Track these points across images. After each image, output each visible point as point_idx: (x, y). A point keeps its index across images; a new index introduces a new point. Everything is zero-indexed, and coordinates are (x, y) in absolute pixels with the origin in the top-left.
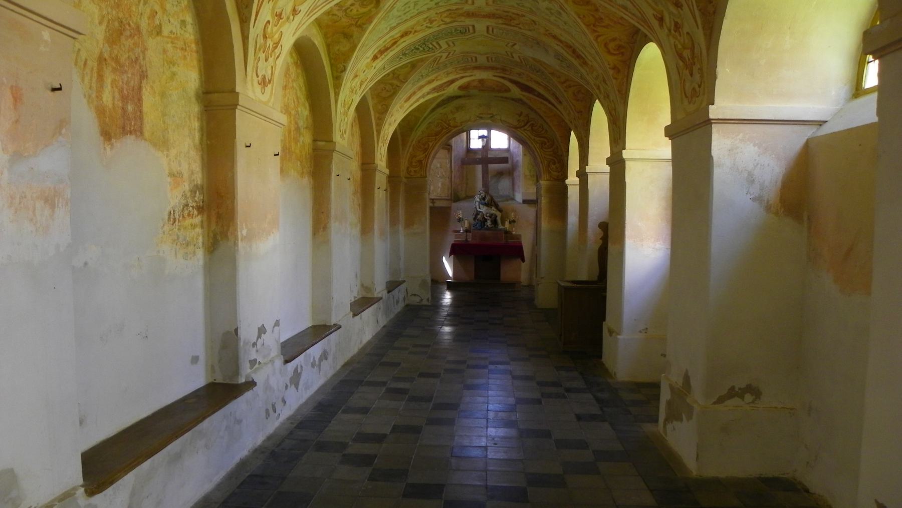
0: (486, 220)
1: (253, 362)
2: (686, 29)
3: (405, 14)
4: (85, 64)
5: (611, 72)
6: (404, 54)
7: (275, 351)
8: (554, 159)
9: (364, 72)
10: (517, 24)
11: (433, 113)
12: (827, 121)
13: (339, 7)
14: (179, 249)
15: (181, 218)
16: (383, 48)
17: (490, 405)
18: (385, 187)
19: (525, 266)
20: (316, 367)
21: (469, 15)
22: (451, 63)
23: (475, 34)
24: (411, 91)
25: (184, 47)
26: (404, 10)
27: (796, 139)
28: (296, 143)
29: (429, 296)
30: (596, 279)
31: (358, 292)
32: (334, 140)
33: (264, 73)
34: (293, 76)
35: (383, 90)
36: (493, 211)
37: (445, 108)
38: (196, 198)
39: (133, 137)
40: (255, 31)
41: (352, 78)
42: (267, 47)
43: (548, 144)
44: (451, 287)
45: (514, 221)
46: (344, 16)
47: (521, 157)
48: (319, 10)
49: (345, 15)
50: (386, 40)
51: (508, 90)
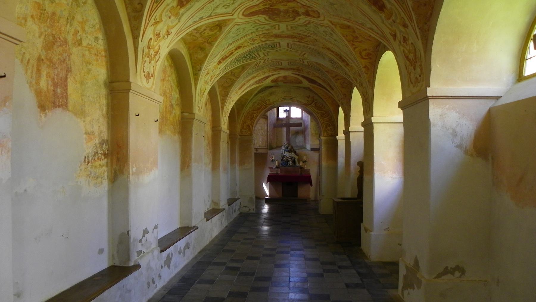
0: (289, 161)
1: (139, 252)
2: (411, 41)
3: (237, 35)
4: (28, 62)
5: (363, 70)
6: (238, 61)
7: (154, 245)
8: (330, 124)
9: (213, 71)
10: (306, 42)
11: (257, 96)
12: (501, 97)
13: (196, 31)
14: (91, 180)
15: (93, 161)
16: (225, 57)
17: (291, 278)
18: (227, 141)
19: (312, 188)
20: (181, 254)
21: (276, 36)
22: (266, 66)
23: (281, 48)
24: (243, 83)
25: (97, 53)
26: (237, 33)
27: (483, 108)
28: (170, 114)
29: (254, 207)
30: (356, 197)
31: (210, 206)
32: (194, 112)
33: (148, 70)
34: (169, 73)
35: (225, 82)
36: (293, 155)
37: (263, 93)
38: (103, 148)
39: (61, 109)
40: (143, 44)
41: (205, 74)
42: (151, 54)
43: (325, 114)
44: (268, 201)
45: (306, 161)
46: (200, 37)
47: (310, 122)
48: (184, 32)
49: (201, 36)
50: (226, 52)
51: (301, 82)
